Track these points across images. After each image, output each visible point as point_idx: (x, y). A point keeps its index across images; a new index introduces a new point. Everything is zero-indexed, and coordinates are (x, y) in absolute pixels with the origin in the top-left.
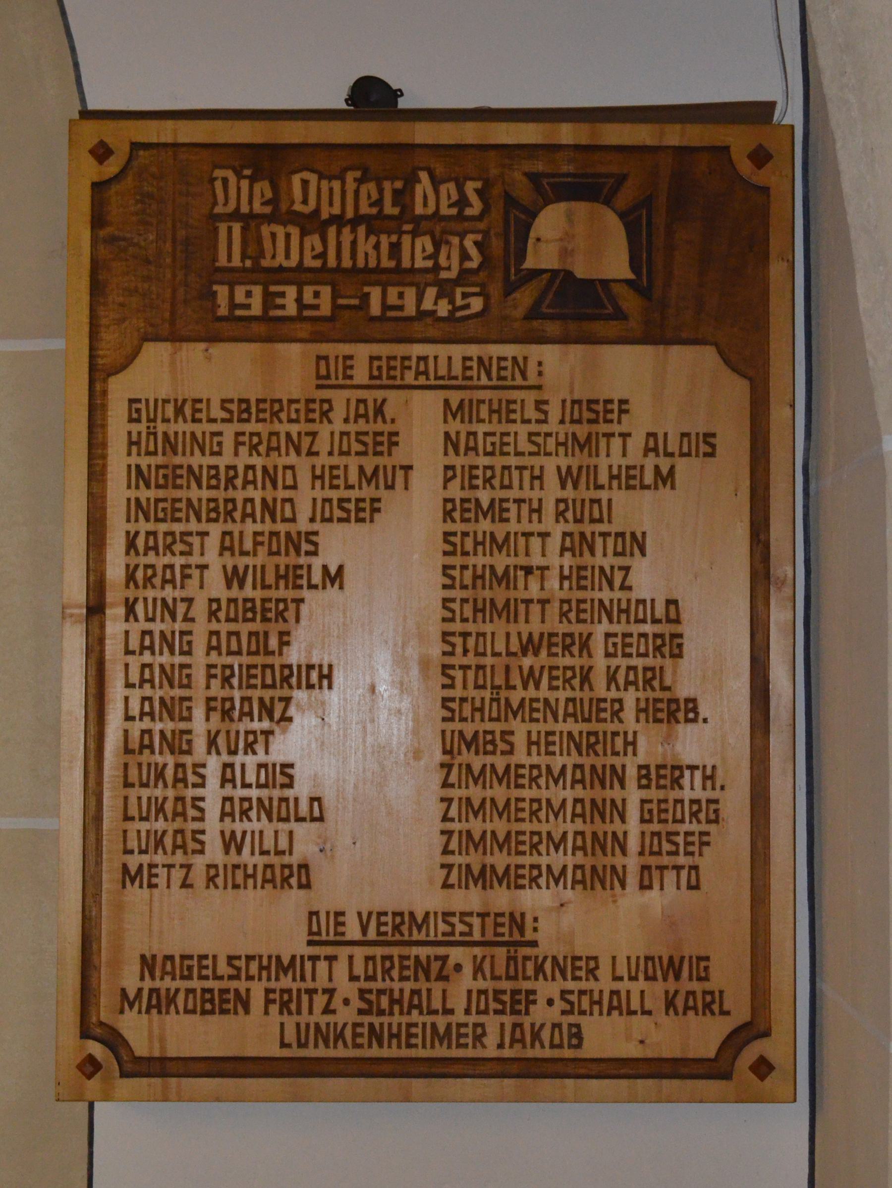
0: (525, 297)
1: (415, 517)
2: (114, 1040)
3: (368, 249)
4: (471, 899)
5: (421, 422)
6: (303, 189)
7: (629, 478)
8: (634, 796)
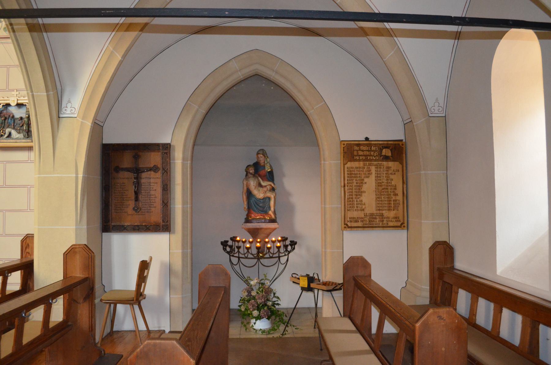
0: (382, 158)
1: (373, 177)
2: (347, 225)
3: (368, 153)
4: (378, 212)
5: (373, 169)
6: (362, 148)
7: (391, 174)
8: (392, 202)
